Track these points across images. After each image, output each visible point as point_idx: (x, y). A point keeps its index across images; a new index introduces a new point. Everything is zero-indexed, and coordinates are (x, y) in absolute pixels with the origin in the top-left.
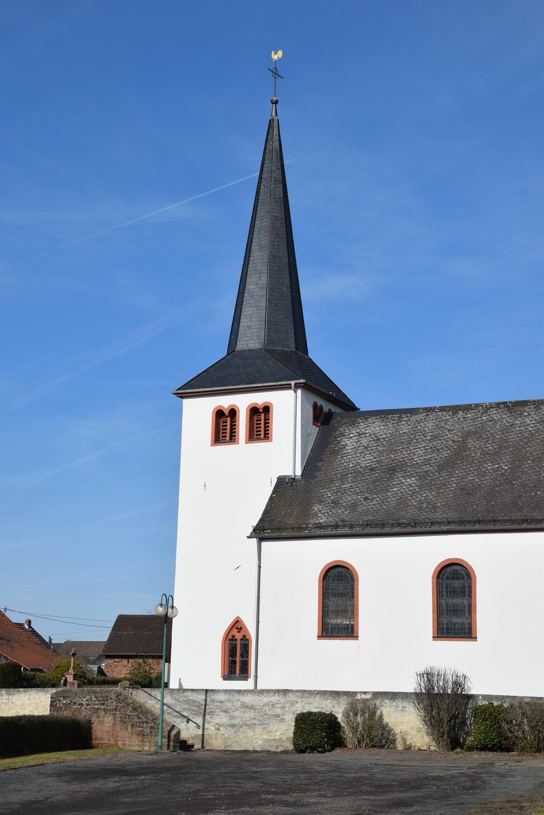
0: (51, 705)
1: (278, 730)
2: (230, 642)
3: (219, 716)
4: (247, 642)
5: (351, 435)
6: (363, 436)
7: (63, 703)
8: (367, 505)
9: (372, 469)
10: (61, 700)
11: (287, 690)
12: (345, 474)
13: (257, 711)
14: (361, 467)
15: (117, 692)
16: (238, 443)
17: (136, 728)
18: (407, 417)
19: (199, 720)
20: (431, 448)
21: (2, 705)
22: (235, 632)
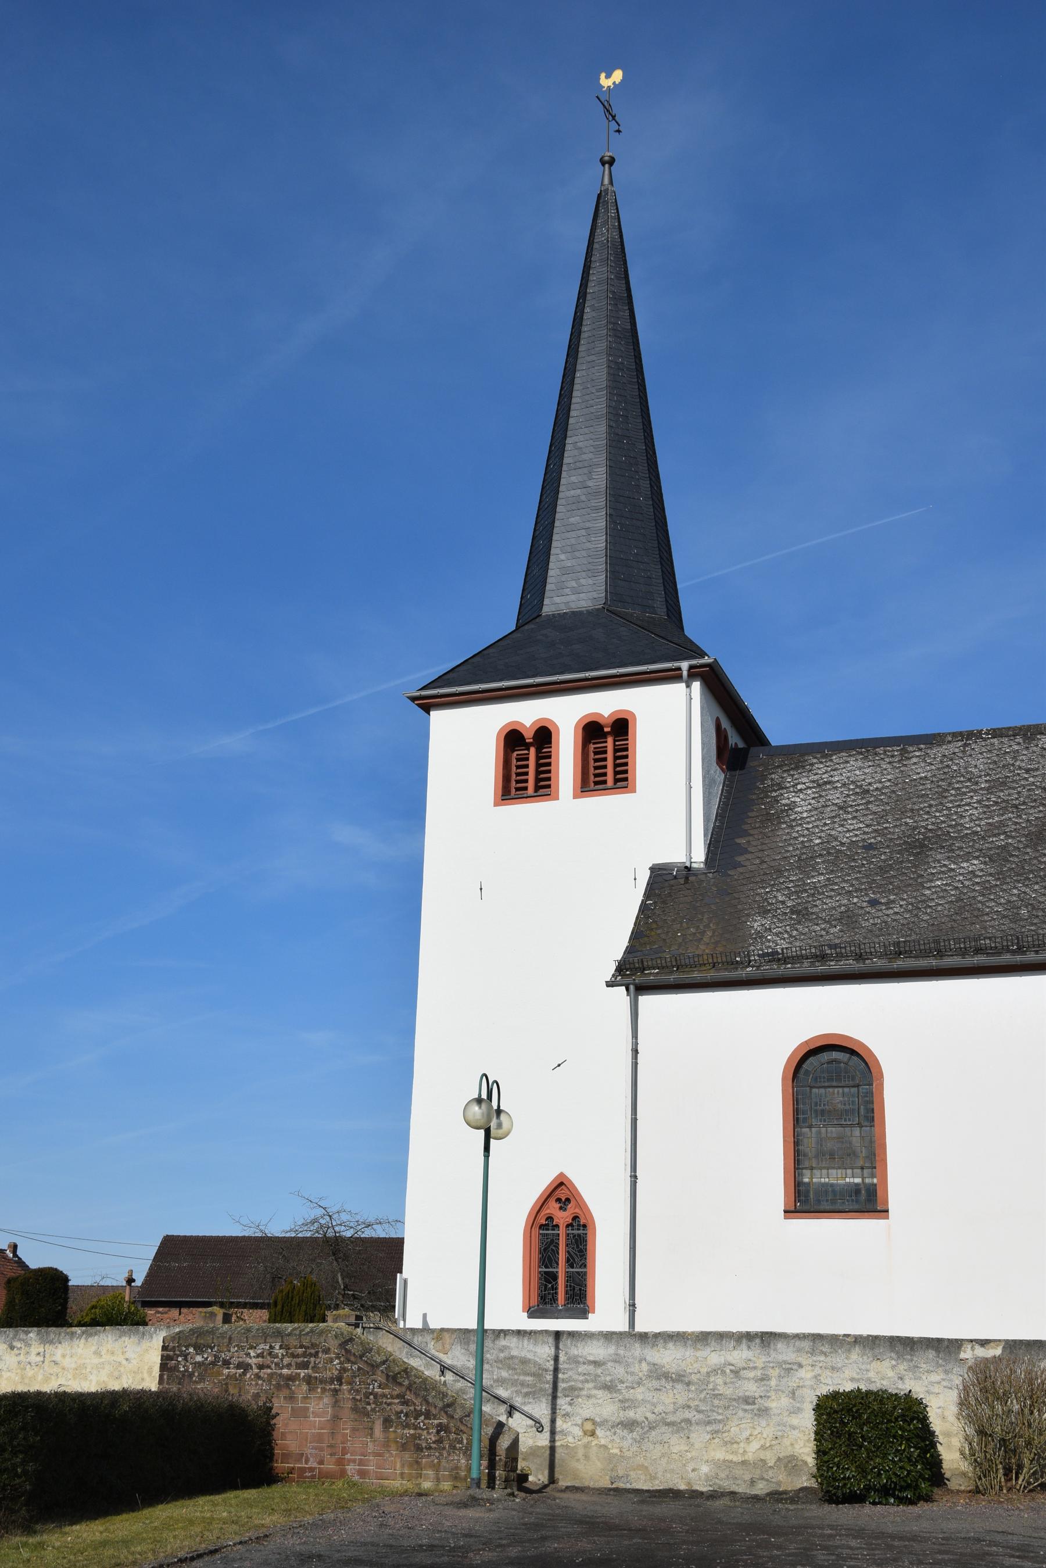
0: (163, 1367)
1: (751, 1438)
2: (541, 1232)
3: (593, 1401)
4: (581, 1232)
5: (799, 787)
6: (828, 786)
7: (195, 1363)
8: (880, 914)
9: (870, 847)
10: (189, 1354)
11: (771, 1333)
12: (807, 858)
13: (693, 1388)
14: (842, 844)
15: (342, 1334)
16: (557, 799)
17: (396, 1428)
18: (920, 750)
19: (541, 1410)
20: (996, 803)
21: (28, 1370)
22: (553, 1208)
